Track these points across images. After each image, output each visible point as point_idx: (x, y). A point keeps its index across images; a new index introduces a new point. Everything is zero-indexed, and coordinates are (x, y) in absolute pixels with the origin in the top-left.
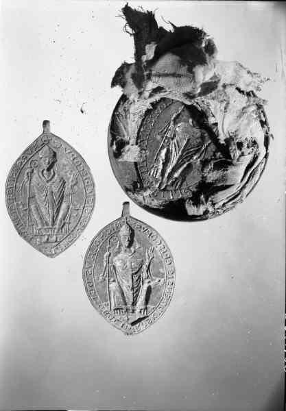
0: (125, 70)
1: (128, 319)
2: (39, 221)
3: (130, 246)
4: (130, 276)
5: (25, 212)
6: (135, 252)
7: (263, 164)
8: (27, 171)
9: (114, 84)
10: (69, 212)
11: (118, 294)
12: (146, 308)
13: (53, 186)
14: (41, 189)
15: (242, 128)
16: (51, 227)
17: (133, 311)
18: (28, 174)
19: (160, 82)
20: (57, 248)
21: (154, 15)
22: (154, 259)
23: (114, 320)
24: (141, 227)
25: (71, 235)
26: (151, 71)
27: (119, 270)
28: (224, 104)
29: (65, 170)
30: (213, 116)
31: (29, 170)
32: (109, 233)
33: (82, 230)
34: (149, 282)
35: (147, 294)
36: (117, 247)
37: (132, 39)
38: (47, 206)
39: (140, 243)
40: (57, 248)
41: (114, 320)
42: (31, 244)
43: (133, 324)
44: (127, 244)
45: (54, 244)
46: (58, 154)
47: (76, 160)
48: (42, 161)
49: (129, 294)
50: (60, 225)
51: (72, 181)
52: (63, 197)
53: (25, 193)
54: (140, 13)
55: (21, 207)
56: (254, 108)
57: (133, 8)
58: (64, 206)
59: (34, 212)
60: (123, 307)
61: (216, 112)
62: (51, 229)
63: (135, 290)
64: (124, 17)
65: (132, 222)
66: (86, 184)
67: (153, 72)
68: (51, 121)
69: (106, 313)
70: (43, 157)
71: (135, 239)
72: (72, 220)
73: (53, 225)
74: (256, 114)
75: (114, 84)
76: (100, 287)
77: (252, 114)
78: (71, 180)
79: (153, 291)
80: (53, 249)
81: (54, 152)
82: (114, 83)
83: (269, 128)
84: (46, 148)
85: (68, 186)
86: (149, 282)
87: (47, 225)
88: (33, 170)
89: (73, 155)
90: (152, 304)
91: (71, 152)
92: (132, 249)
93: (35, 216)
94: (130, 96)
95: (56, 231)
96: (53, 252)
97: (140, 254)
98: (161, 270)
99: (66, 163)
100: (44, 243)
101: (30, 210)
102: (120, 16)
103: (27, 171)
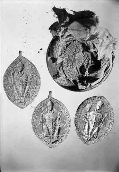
1: (51, 141)
2: (17, 94)
3: (51, 110)
4: (52, 123)
6: (54, 112)
8: (12, 72)
11: (47, 131)
12: (58, 136)
14: (18, 80)
15: (107, 53)
16: (22, 96)
18: (12, 73)
21: (66, 10)
23: (44, 141)
24: (56, 102)
25: (30, 99)
26: (68, 27)
27: (47, 120)
32: (43, 104)
33: (35, 97)
34: (60, 125)
35: (59, 130)
36: (46, 110)
39: (56, 109)
41: (44, 141)
42: (14, 103)
43: (53, 143)
44: (50, 109)
45: (23, 103)
46: (25, 65)
47: (32, 68)
49: (51, 130)
50: (26, 95)
51: (31, 76)
52: (27, 83)
53: (11, 82)
54: (60, 9)
55: (10, 87)
56: (112, 45)
58: (27, 87)
60: (49, 136)
63: (54, 129)
64: (53, 11)
65: (53, 100)
66: (37, 78)
67: (69, 28)
68: (22, 51)
69: (42, 138)
70: (19, 66)
71: (54, 107)
72: (31, 93)
73: (23, 95)
76: (39, 127)
79: (61, 129)
80: (23, 105)
84: (20, 62)
86: (60, 125)
87: (20, 95)
88: (14, 72)
89: (31, 65)
90: (61, 135)
92: (53, 111)
93: (15, 91)
95: (24, 97)
97: (56, 113)
98: (65, 120)
100: (19, 103)
103: (12, 72)
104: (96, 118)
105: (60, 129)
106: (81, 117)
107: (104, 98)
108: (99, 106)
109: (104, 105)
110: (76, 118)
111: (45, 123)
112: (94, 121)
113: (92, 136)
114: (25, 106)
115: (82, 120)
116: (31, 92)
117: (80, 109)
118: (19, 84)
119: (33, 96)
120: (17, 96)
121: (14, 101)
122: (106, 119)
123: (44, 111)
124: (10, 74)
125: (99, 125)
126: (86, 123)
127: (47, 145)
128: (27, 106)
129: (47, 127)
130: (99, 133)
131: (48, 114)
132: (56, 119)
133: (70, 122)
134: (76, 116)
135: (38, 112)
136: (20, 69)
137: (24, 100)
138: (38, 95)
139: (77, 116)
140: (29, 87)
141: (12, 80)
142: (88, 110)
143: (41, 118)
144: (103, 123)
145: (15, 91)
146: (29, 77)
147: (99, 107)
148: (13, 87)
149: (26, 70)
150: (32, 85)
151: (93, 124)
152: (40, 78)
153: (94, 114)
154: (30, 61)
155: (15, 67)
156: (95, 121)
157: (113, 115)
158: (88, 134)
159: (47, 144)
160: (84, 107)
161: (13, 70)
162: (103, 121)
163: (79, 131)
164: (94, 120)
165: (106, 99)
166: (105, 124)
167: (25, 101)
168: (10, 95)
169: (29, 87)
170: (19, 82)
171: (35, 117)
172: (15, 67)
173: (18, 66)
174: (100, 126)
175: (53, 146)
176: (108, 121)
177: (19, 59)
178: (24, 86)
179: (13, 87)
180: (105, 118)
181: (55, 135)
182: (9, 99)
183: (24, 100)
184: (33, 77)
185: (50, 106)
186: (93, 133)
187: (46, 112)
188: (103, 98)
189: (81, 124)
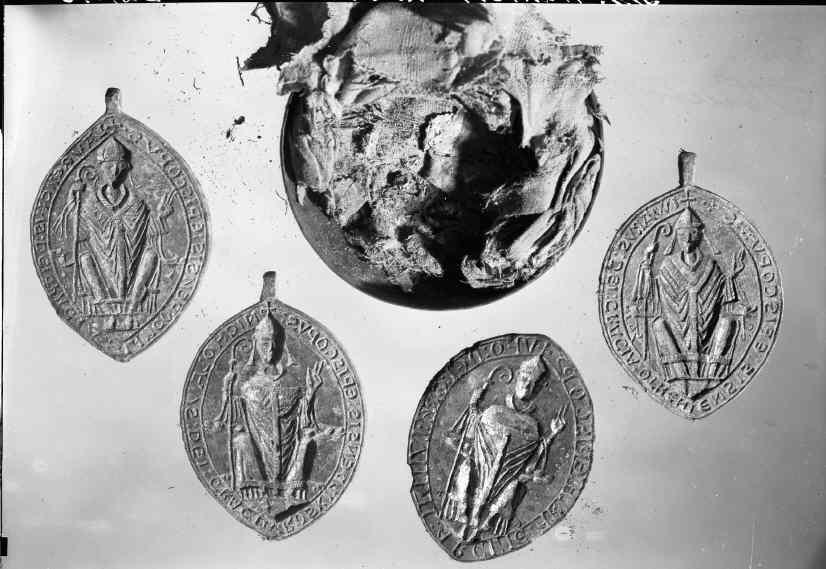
1: (269, 508)
2: (97, 289)
3: (274, 361)
4: (274, 422)
5: (68, 269)
6: (285, 372)
8: (73, 188)
10: (158, 268)
11: (249, 458)
13: (124, 218)
14: (100, 226)
16: (119, 299)
18: (74, 193)
22: (323, 387)
23: (241, 509)
27: (253, 408)
29: (148, 187)
32: (232, 336)
33: (183, 307)
34: (312, 434)
36: (250, 362)
38: (113, 258)
39: (296, 356)
41: (241, 509)
43: (280, 517)
44: (268, 356)
46: (134, 155)
49: (272, 458)
50: (137, 296)
51: (163, 209)
53: (70, 233)
55: (61, 260)
58: (147, 257)
62: (120, 303)
63: (284, 449)
69: (227, 495)
70: (105, 158)
72: (163, 286)
73: (124, 295)
76: (213, 442)
78: (159, 207)
84: (111, 143)
86: (312, 434)
87: (113, 295)
88: (85, 186)
90: (317, 479)
92: (279, 366)
95: (131, 307)
96: (126, 352)
98: (336, 410)
99: (149, 171)
100: (109, 331)
101: (79, 266)
104: (509, 437)
105: (315, 453)
106: (440, 430)
107: (551, 343)
108: (525, 380)
109: (552, 377)
110: (415, 435)
111: (241, 423)
112: (500, 455)
113: (486, 522)
114: (135, 349)
115: (444, 444)
116: (162, 282)
117: (437, 394)
118: (107, 242)
119: (173, 303)
120: (99, 298)
122: (558, 444)
123: (238, 366)
125: (522, 471)
126: (460, 459)
127: (252, 528)
128: (144, 348)
129: (253, 441)
130: (521, 509)
131: (260, 378)
132: (298, 402)
133: (359, 417)
134: (415, 422)
135: (211, 370)
137: (132, 322)
139: (419, 426)
140: (156, 258)
141: (75, 226)
142: (473, 401)
143: (225, 398)
144: (543, 464)
146: (151, 213)
147: (528, 387)
148: (77, 255)
150: (169, 247)
151: (496, 467)
152: (205, 216)
153: (500, 418)
156: (504, 451)
157: (590, 430)
158: (468, 512)
159: (253, 523)
160: (459, 385)
161: (78, 178)
162: (541, 451)
163: (424, 495)
164: (500, 445)
165: (560, 349)
166: (549, 471)
167: (135, 324)
168: (63, 295)
169: (156, 258)
170: (108, 232)
171: (196, 392)
174: (527, 477)
175: (282, 533)
176: (568, 456)
177: (105, 127)
178: (132, 252)
179: (77, 255)
180: (552, 440)
181: (289, 478)
182: (58, 313)
183: (132, 322)
185: (270, 343)
186: (494, 509)
187: (246, 368)
188: (548, 345)
189: (437, 461)
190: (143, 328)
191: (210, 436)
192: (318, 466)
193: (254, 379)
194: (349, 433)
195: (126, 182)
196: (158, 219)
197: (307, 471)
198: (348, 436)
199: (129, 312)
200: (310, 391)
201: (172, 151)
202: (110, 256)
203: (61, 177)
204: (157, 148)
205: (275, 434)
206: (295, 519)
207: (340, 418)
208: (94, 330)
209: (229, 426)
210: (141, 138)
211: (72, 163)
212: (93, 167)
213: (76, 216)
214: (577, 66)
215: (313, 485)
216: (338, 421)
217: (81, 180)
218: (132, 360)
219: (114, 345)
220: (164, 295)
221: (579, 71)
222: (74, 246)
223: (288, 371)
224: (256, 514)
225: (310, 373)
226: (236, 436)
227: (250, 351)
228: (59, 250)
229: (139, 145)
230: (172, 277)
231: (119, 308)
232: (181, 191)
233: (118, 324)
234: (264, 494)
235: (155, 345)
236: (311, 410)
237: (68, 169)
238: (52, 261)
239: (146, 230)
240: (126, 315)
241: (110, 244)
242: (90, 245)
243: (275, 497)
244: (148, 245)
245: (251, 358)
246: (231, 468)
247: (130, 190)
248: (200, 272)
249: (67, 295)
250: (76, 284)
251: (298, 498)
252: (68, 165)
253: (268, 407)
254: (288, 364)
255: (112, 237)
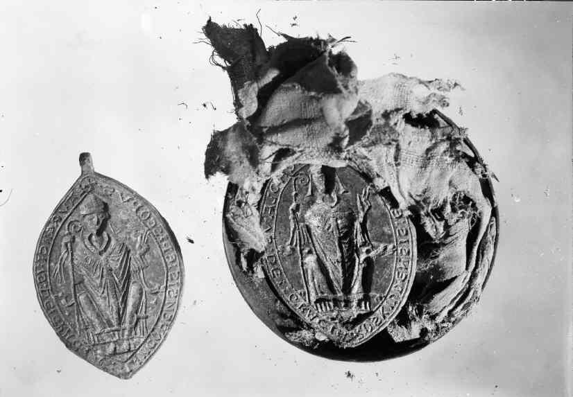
0: (220, 144)
3: (328, 190)
5: (71, 309)
6: (339, 199)
7: (494, 227)
9: (209, 171)
10: (144, 297)
13: (110, 259)
14: (93, 267)
16: (116, 327)
17: (348, 303)
18: (66, 244)
19: (283, 139)
20: (132, 362)
22: (372, 210)
27: (317, 232)
28: (393, 150)
29: (125, 231)
30: (378, 176)
31: (66, 240)
33: (169, 326)
34: (368, 252)
36: (309, 193)
37: (225, 76)
38: (105, 294)
39: (346, 184)
40: (132, 362)
46: (111, 206)
47: (141, 212)
48: (86, 220)
49: (337, 274)
50: (131, 323)
51: (141, 247)
53: (67, 278)
54: (234, 30)
55: (63, 301)
57: (220, 24)
58: (133, 289)
59: (86, 307)
61: (382, 170)
62: (118, 330)
64: (208, 41)
72: (150, 311)
73: (119, 324)
74: (451, 156)
75: (209, 171)
77: (445, 158)
78: (137, 246)
80: (126, 365)
81: (104, 203)
82: (209, 170)
83: (484, 166)
84: (91, 197)
85: (135, 256)
86: (368, 252)
87: (111, 325)
88: (74, 238)
91: (132, 199)
92: (334, 195)
93: (89, 314)
94: (243, 182)
95: (126, 333)
96: (128, 370)
98: (386, 229)
99: (125, 218)
100: (111, 355)
101: (79, 305)
102: (201, 41)
111: (308, 246)
114: (134, 367)
118: (98, 281)
119: (160, 324)
121: (88, 351)
123: (299, 197)
124: (56, 248)
128: (142, 365)
131: (320, 205)
133: (407, 234)
136: (92, 224)
137: (130, 345)
138: (178, 316)
141: (71, 273)
145: (89, 314)
146: (132, 252)
148: (75, 296)
149: (119, 226)
154: (127, 188)
155: (71, 219)
161: (67, 232)
167: (132, 346)
168: (69, 331)
169: (141, 289)
170: (98, 273)
172: (71, 219)
173: (84, 213)
178: (121, 287)
179: (75, 296)
182: (67, 346)
183: (130, 345)
184: (148, 249)
187: (307, 199)
190: (138, 349)
191: (284, 258)
192: (376, 280)
193: (315, 207)
194: (399, 249)
195: (107, 229)
196: (138, 256)
197: (367, 284)
198: (399, 251)
199: (125, 337)
200: (362, 214)
201: (142, 198)
202: (103, 293)
203: (53, 233)
204: (128, 198)
205: (339, 254)
206: (363, 327)
207: (390, 236)
208: (98, 356)
209: (298, 248)
210: (114, 190)
211: (61, 219)
212: (78, 221)
213: (70, 264)
214: (444, 146)
215: (374, 296)
216: (389, 239)
217: (70, 233)
218: (133, 377)
219: (117, 366)
220: (153, 319)
221: (445, 152)
222: (72, 290)
223: (342, 197)
224: (330, 324)
225: (360, 199)
226: (305, 257)
227: (307, 184)
228: (60, 294)
229: (112, 197)
230: (156, 303)
231: (117, 336)
232: (153, 231)
233: (118, 348)
234: (334, 306)
235: (150, 361)
236: (364, 231)
237: (57, 226)
238: (56, 304)
239: (129, 267)
240: (123, 340)
241: (101, 282)
242: (85, 286)
243: (344, 309)
244: (133, 280)
245: (310, 190)
246: (305, 285)
247: (111, 235)
248: (179, 294)
249: (72, 330)
250: (78, 320)
251: (363, 308)
252: (57, 221)
253: (330, 230)
254: (341, 192)
255: (102, 276)
